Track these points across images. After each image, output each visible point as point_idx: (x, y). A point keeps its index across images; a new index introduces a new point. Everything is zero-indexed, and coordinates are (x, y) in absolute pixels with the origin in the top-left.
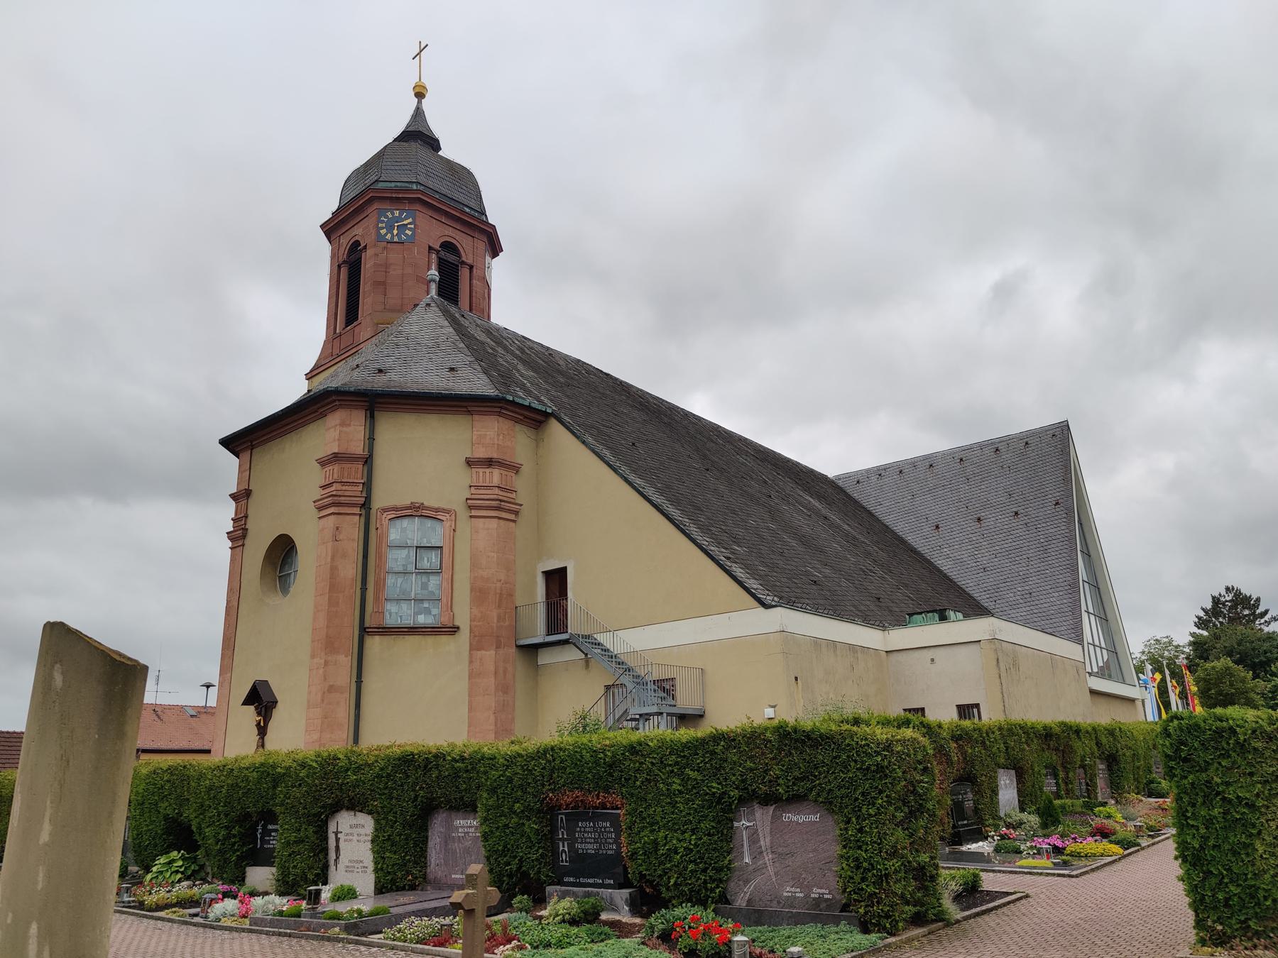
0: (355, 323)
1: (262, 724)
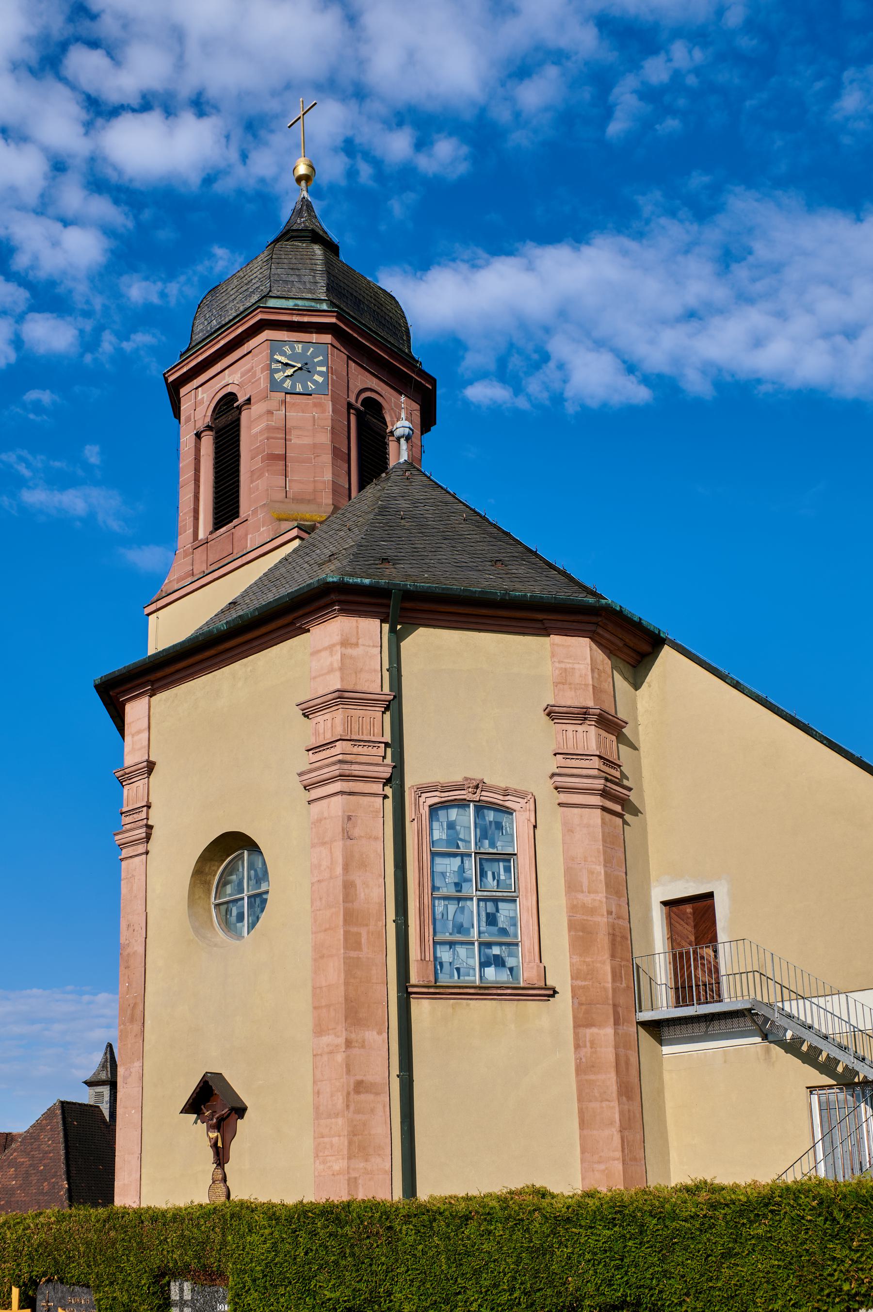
0: (235, 522)
1: (220, 1144)
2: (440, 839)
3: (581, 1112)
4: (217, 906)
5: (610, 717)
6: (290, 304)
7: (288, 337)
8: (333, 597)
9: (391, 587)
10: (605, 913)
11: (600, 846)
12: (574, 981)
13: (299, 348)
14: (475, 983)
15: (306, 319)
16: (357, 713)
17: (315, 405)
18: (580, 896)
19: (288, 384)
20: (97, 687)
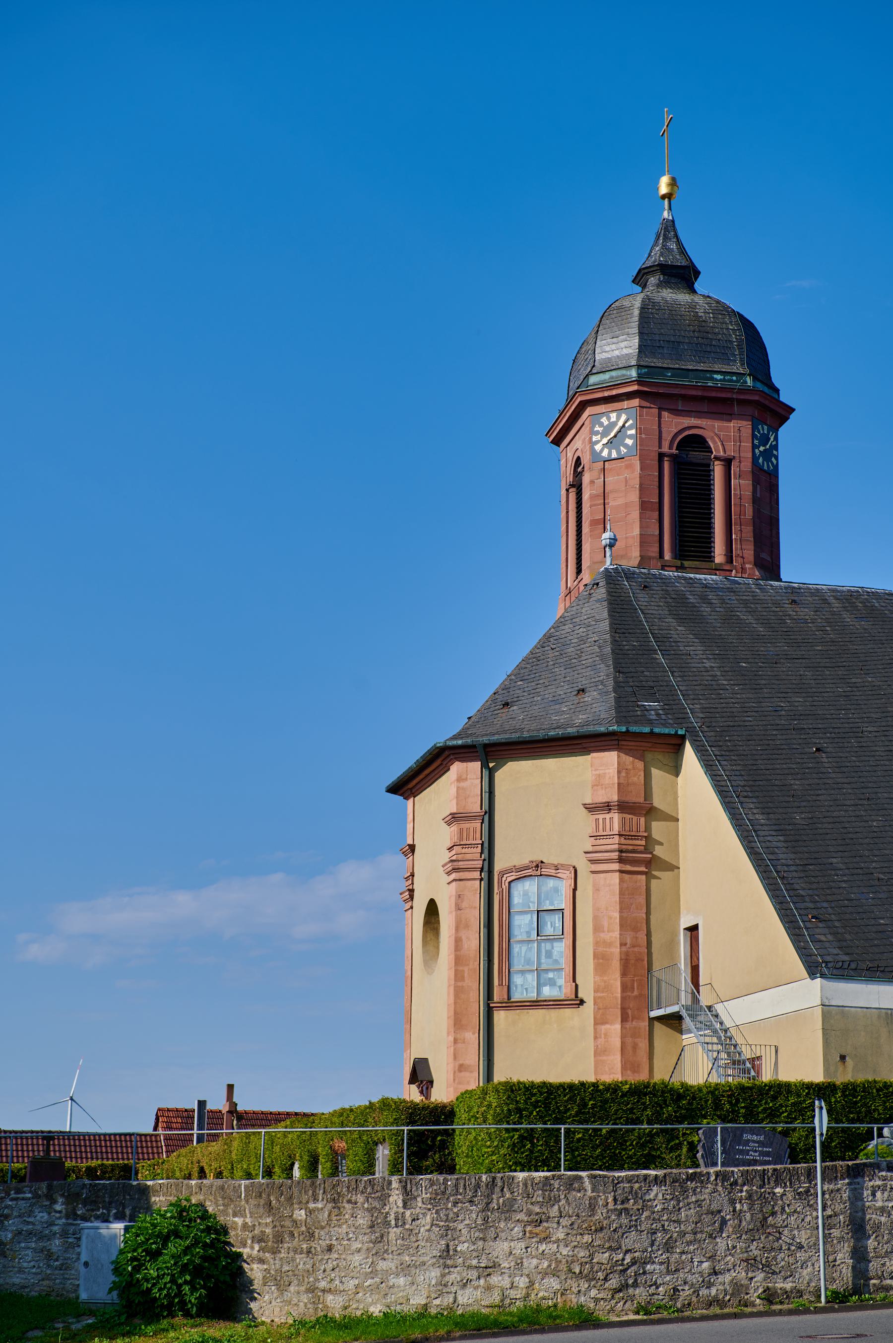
2: (518, 903)
7: (605, 409)
8: (447, 753)
9: (474, 743)
16: (465, 825)
18: (602, 935)
19: (605, 453)
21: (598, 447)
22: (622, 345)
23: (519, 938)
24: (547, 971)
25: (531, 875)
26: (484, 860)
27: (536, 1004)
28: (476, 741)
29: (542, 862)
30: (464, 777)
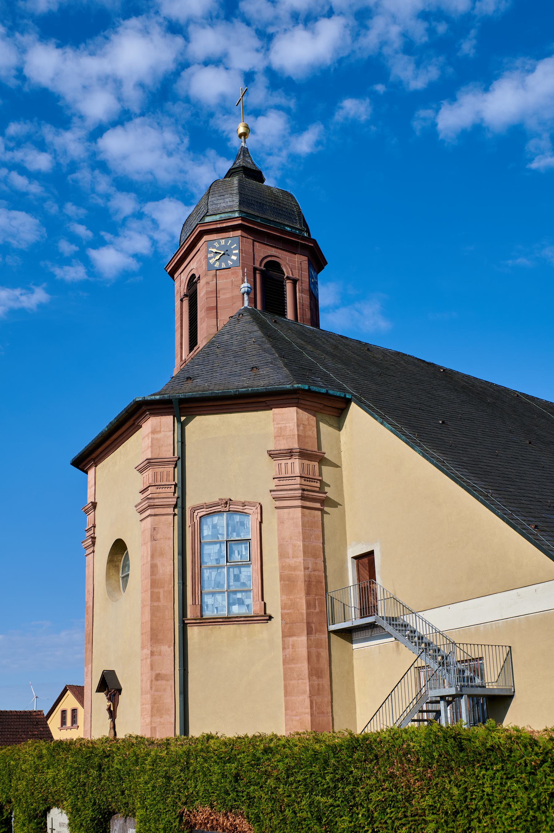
1: (112, 709)
2: (208, 535)
3: (286, 687)
4: (123, 578)
5: (309, 452)
6: (217, 217)
7: (217, 237)
8: (144, 408)
9: (171, 398)
10: (303, 569)
11: (300, 529)
12: (283, 611)
13: (223, 242)
14: (225, 615)
15: (224, 225)
16: (159, 470)
17: (233, 274)
18: (287, 560)
19: (217, 265)
20: (72, 464)
21: (212, 261)
22: (227, 200)
23: (209, 564)
24: (235, 592)
25: (221, 511)
26: (178, 498)
27: (228, 620)
28: (173, 396)
29: (230, 500)
30: (158, 429)
